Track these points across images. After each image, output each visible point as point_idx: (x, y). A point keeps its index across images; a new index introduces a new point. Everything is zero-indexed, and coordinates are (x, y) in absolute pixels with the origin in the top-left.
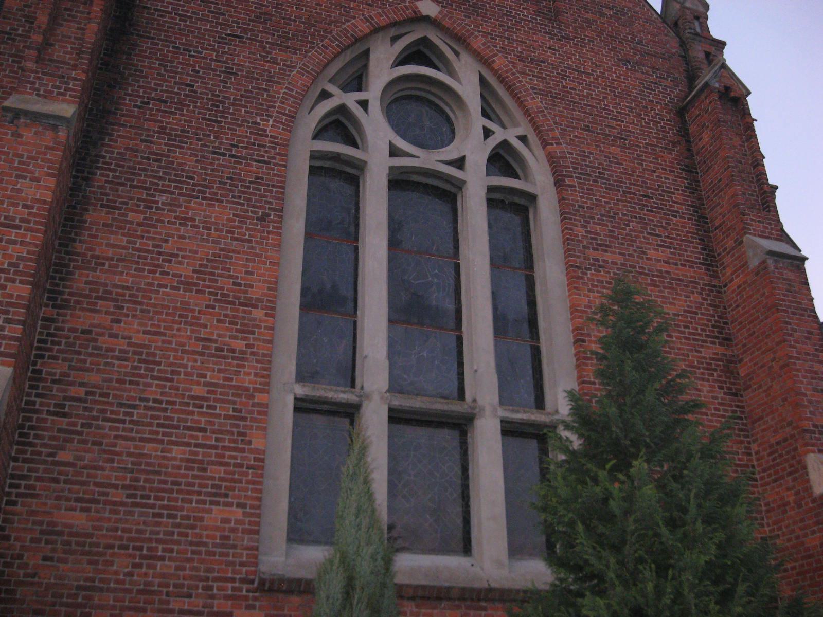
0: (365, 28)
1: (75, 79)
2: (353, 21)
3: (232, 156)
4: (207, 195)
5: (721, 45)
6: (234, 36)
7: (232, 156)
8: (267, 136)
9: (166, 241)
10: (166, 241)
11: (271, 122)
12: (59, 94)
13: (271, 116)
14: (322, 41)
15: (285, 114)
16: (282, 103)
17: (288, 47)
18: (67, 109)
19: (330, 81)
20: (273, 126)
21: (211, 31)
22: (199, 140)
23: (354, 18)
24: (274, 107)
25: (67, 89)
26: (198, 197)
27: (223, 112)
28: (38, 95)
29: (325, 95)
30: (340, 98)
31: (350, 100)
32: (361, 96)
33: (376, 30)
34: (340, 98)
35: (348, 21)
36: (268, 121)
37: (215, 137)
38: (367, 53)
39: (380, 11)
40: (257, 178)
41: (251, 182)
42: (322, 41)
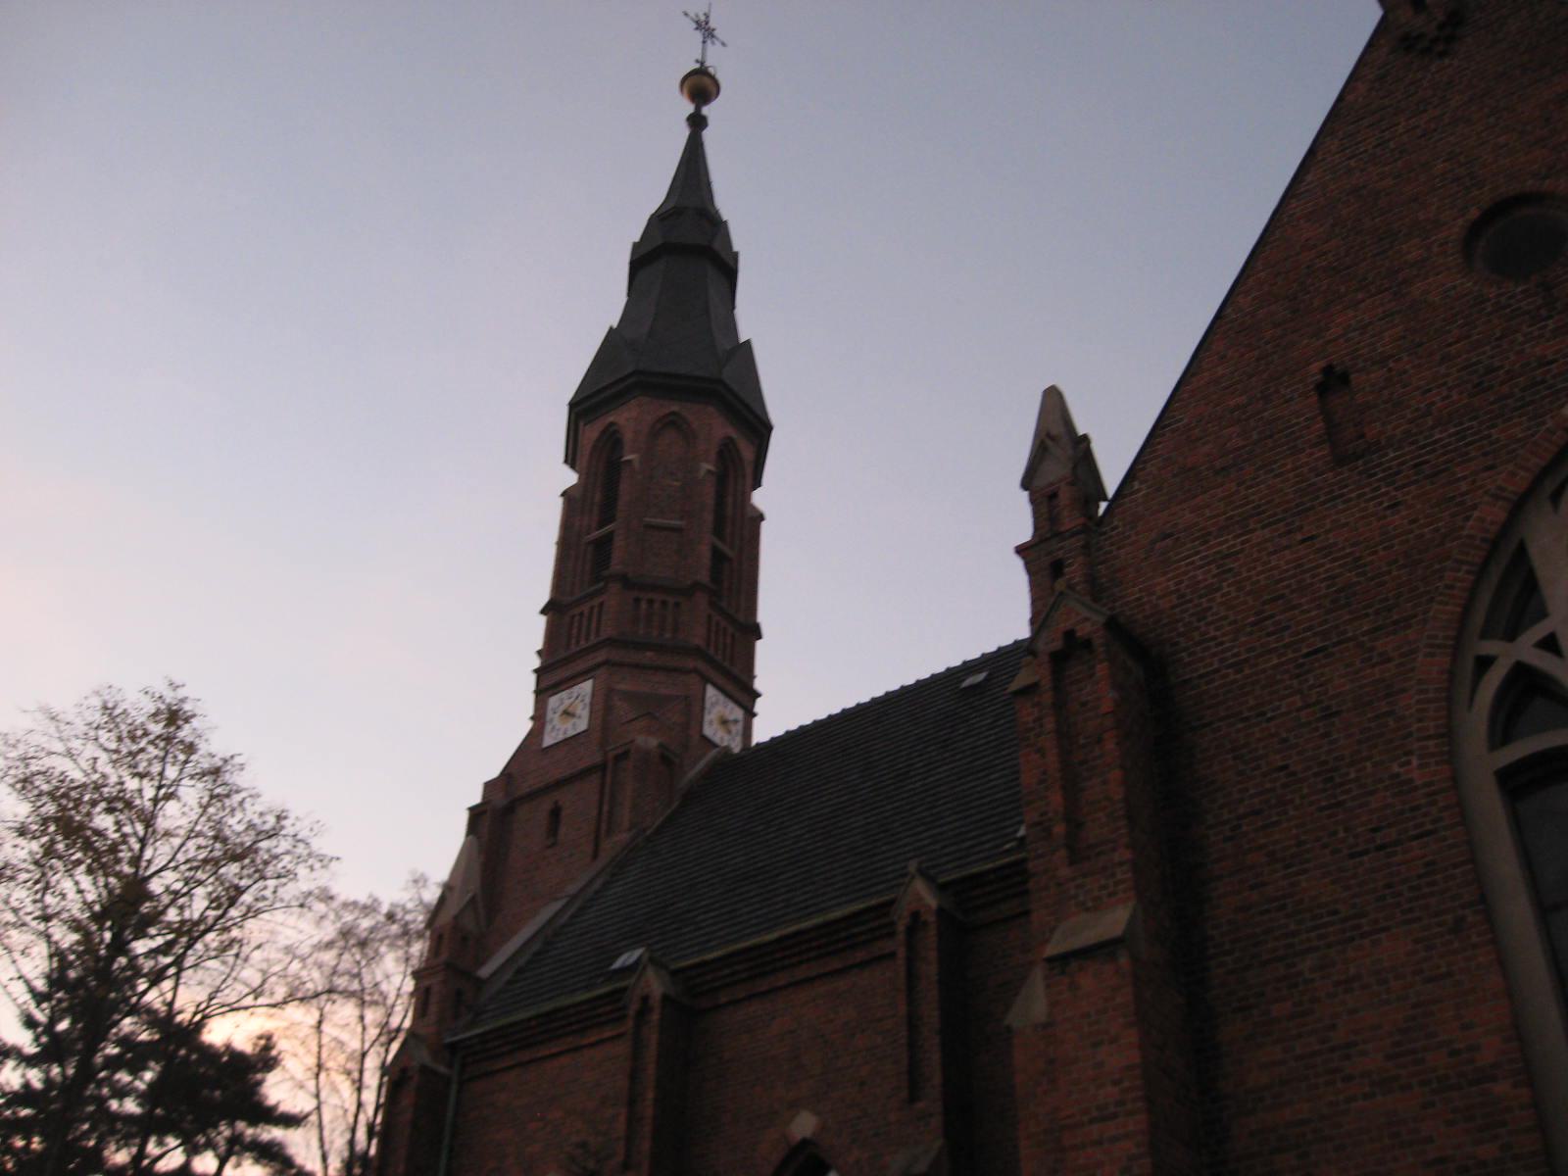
0: (1499, 513)
1: (1121, 864)
2: (1476, 514)
3: (1380, 848)
4: (1366, 928)
5: (532, 718)
6: (1316, 652)
7: (1380, 848)
8: (1416, 788)
9: (1333, 1027)
10: (1333, 1027)
11: (1415, 762)
12: (1110, 895)
13: (1409, 753)
14: (1441, 578)
15: (1429, 737)
16: (1420, 720)
17: (1395, 623)
18: (1115, 920)
19: (1485, 635)
20: (1421, 766)
21: (1282, 664)
22: (1325, 846)
23: (1474, 507)
24: (1410, 734)
25: (1116, 884)
26: (1353, 939)
27: (1342, 784)
28: (1087, 910)
29: (1484, 663)
30: (1507, 655)
31: (1525, 649)
32: (1539, 631)
33: (1518, 507)
34: (1507, 655)
35: (1468, 518)
36: (1409, 763)
37: (1346, 830)
38: (1522, 549)
39: (1510, 467)
40: (1428, 864)
41: (1420, 877)
42: (1441, 578)
